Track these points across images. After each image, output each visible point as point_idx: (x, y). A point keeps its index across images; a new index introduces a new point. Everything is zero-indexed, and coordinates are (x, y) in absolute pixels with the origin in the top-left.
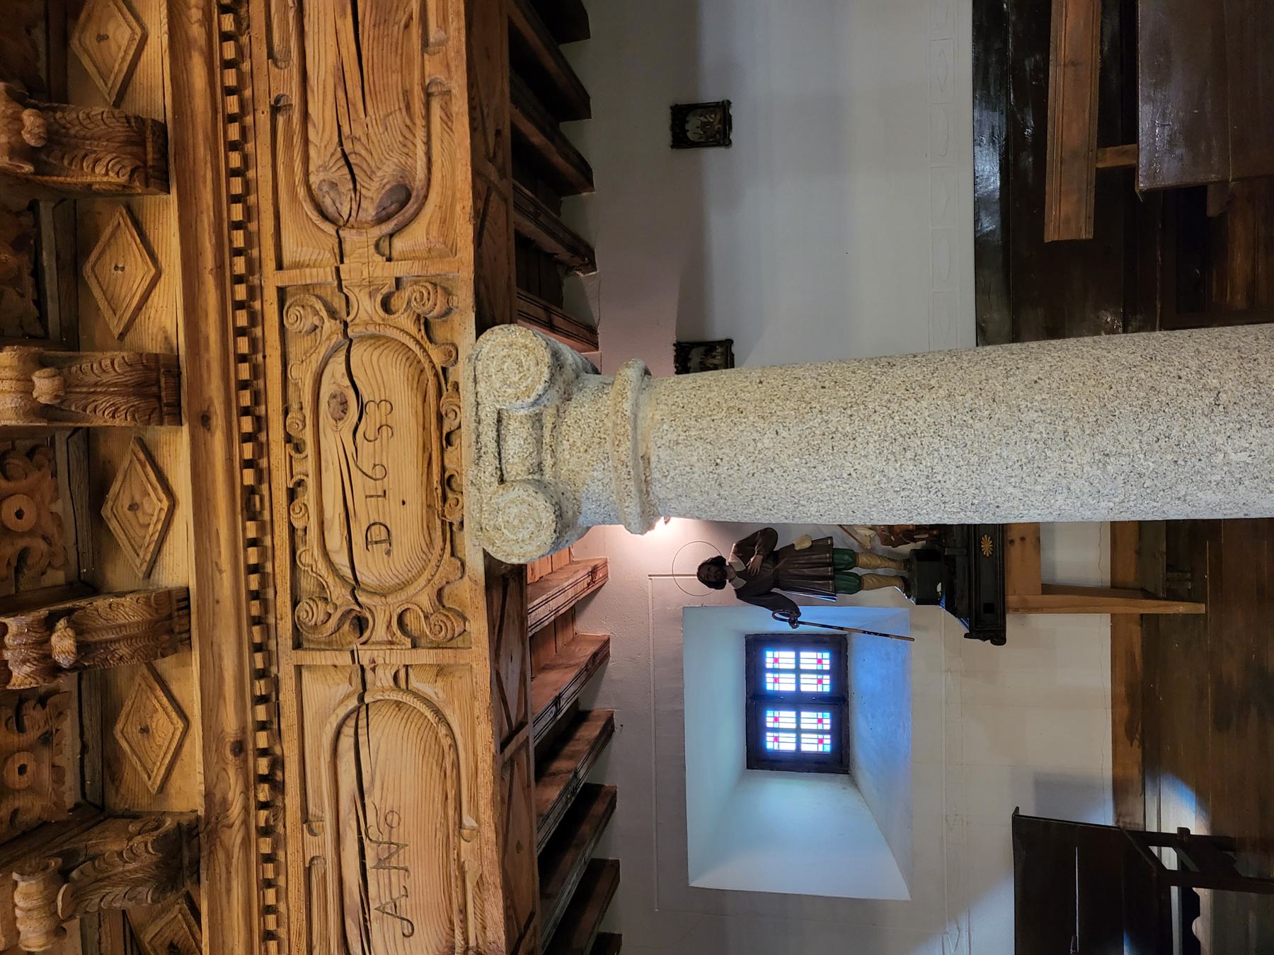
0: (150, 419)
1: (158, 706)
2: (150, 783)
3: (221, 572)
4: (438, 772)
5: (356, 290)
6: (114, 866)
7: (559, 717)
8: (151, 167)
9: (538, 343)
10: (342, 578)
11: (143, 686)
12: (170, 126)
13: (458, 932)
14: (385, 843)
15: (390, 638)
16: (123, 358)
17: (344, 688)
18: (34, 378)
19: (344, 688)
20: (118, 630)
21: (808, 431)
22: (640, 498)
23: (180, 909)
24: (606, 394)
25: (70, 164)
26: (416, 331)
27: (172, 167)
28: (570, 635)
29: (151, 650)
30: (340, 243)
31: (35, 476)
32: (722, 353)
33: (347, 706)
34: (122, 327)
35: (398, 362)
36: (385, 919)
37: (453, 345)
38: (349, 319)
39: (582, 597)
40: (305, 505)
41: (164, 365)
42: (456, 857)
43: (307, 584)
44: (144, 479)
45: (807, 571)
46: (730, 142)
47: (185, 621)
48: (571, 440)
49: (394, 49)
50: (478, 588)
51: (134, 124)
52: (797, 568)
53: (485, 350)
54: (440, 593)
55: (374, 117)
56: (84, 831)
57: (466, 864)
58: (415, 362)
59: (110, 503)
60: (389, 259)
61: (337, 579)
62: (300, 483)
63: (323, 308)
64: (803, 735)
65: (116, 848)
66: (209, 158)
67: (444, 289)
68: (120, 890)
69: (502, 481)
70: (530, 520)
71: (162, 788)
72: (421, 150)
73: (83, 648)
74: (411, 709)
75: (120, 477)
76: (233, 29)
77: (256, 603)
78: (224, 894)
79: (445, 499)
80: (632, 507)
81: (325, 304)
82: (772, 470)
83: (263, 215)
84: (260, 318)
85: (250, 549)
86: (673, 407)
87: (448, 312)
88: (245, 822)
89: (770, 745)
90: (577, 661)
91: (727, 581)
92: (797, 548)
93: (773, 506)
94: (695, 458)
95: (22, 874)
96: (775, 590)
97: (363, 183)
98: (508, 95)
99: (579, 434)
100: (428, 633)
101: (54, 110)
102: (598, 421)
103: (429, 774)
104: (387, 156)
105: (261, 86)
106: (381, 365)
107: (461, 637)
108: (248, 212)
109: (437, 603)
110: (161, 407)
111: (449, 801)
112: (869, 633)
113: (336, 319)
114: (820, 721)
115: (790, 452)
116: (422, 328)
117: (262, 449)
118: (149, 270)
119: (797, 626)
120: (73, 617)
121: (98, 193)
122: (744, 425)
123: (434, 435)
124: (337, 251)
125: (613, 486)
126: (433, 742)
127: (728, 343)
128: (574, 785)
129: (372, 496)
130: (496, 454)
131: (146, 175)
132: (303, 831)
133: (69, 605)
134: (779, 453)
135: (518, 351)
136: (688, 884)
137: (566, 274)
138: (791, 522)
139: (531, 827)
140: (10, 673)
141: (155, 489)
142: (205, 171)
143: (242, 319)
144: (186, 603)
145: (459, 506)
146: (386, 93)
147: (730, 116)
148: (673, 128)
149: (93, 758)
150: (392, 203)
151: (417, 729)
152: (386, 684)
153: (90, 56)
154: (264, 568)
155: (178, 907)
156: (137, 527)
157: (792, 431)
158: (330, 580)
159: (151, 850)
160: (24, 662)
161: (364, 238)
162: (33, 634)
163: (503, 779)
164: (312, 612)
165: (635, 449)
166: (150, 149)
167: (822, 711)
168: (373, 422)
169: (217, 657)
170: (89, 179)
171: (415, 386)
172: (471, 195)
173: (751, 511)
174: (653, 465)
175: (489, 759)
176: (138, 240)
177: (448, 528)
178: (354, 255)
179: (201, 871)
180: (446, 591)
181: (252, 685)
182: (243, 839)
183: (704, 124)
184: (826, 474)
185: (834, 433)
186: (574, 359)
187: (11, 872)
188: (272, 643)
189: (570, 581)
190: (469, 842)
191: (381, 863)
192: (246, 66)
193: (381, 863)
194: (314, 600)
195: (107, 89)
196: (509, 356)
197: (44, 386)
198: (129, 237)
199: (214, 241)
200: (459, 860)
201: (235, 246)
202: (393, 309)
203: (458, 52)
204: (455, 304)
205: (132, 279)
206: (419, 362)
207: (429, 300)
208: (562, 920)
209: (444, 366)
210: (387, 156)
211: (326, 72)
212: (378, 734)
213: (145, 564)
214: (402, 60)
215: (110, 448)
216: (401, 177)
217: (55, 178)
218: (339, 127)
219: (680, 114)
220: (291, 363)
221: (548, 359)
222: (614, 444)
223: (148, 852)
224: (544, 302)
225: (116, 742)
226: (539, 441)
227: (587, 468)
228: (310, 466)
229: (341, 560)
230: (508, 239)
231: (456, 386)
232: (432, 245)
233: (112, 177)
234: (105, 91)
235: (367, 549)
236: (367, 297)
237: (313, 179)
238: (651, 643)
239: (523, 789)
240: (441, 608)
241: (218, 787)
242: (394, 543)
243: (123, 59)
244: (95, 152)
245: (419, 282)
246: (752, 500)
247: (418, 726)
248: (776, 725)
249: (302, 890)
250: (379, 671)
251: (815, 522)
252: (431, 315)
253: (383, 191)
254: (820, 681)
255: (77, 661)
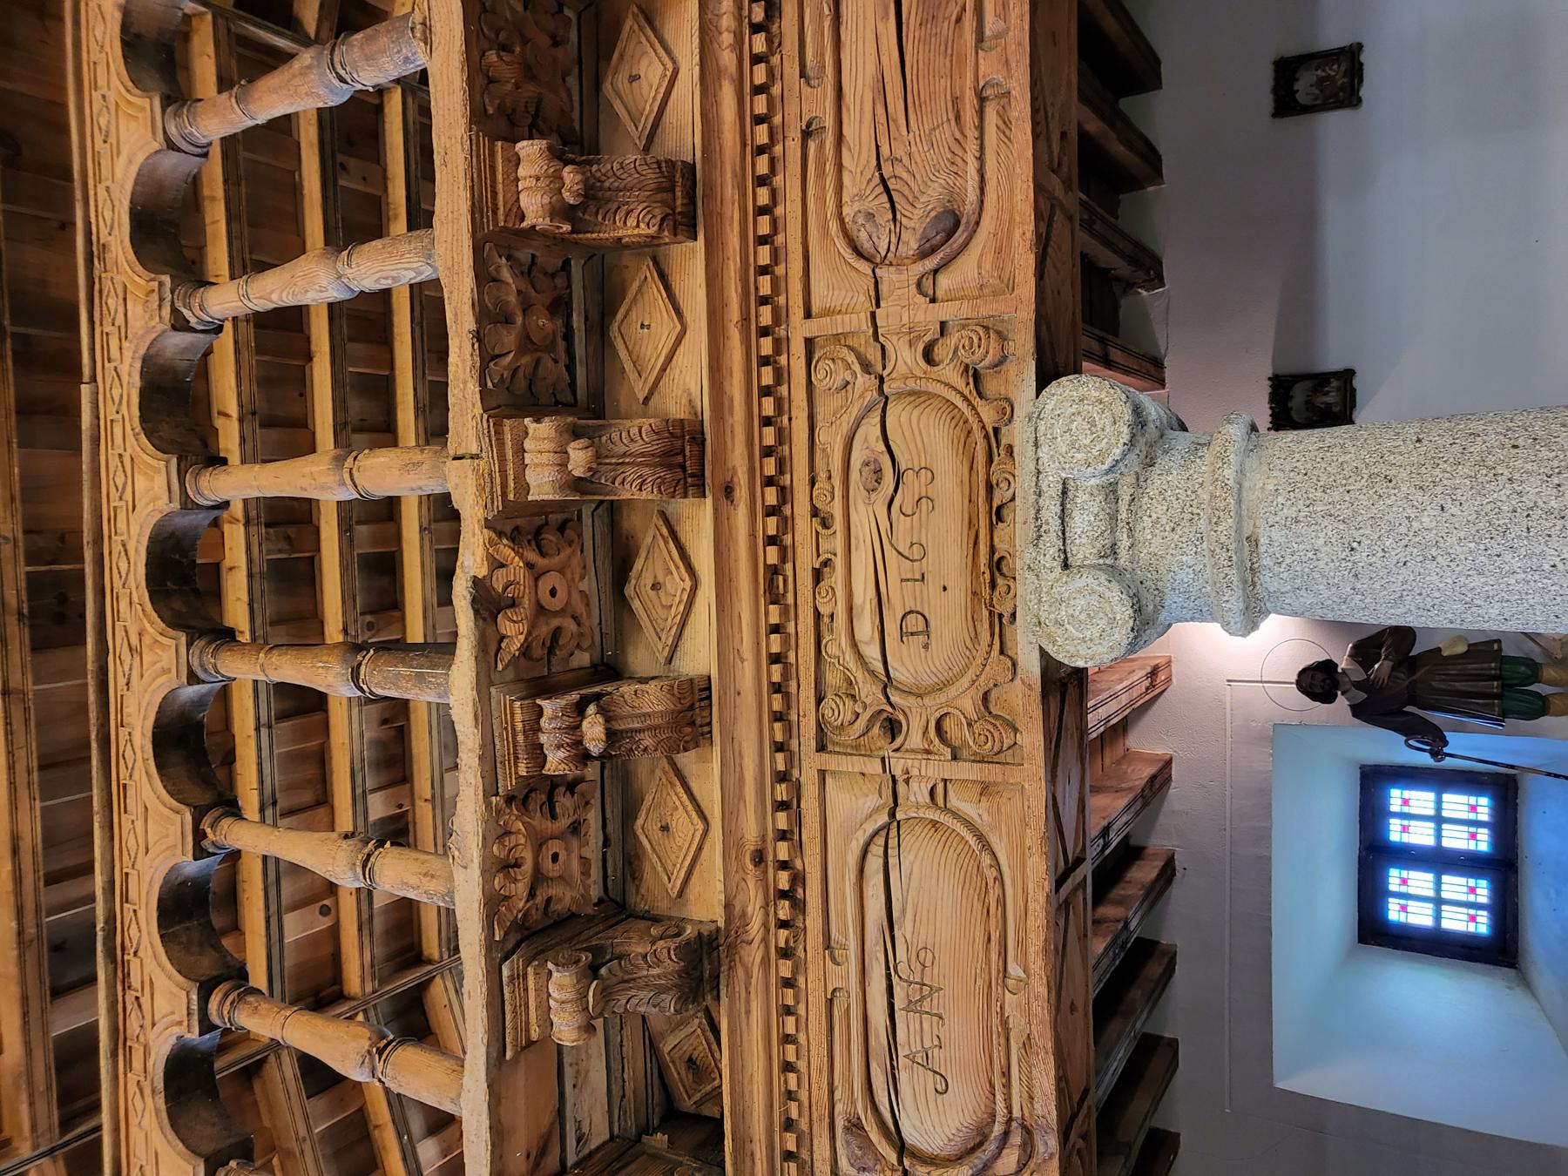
0: (675, 491)
1: (678, 803)
2: (670, 886)
3: (742, 661)
4: (980, 908)
5: (894, 339)
6: (640, 969)
7: (1107, 852)
8: (679, 213)
9: (1115, 396)
10: (873, 673)
11: (664, 780)
12: (698, 167)
13: (999, 1097)
14: (917, 983)
15: (926, 746)
16: (650, 425)
17: (873, 801)
18: (569, 450)
19: (873, 801)
20: (643, 719)
21: (1489, 507)
22: (1244, 590)
23: (700, 1023)
24: (1200, 457)
25: (604, 219)
26: (964, 385)
27: (700, 212)
28: (1120, 751)
29: (675, 742)
30: (876, 283)
31: (567, 552)
32: (1339, 389)
33: (876, 821)
34: (647, 391)
35: (942, 422)
36: (915, 1069)
37: (1007, 400)
38: (885, 373)
39: (1140, 703)
40: (833, 589)
41: (689, 433)
42: (999, 1010)
43: (833, 679)
44: (668, 558)
45: (1459, 686)
46: (1360, 100)
47: (705, 713)
48: (1154, 516)
49: (943, 48)
50: (1033, 693)
51: (664, 169)
52: (1444, 680)
53: (1049, 407)
54: (986, 697)
55: (917, 133)
56: (610, 927)
57: (1011, 1020)
58: (962, 421)
59: (633, 582)
60: (933, 301)
61: (867, 675)
62: (826, 563)
63: (855, 361)
64: (1444, 907)
65: (640, 950)
66: (737, 197)
67: (998, 333)
68: (645, 995)
69: (1066, 566)
70: (1101, 615)
71: (681, 893)
72: (972, 169)
73: (612, 736)
74: (949, 831)
75: (643, 554)
76: (764, 49)
77: (778, 697)
78: (743, 1015)
79: (993, 585)
80: (1234, 601)
81: (859, 356)
82: (1434, 558)
83: (790, 256)
84: (786, 375)
85: (773, 636)
86: (1292, 474)
87: (1002, 360)
88: (765, 940)
89: (1394, 913)
90: (1131, 784)
91: (1339, 693)
92: (1445, 654)
93: (1433, 606)
94: (1321, 541)
95: (557, 965)
96: (1409, 709)
97: (903, 211)
98: (1075, 87)
99: (1165, 508)
100: (971, 743)
101: (590, 163)
102: (1189, 492)
103: (969, 910)
104: (933, 178)
105: (792, 109)
106: (922, 426)
107: (1011, 751)
108: (775, 255)
109: (982, 708)
110: (685, 478)
111: (993, 943)
112: (1557, 776)
113: (870, 374)
114: (1472, 890)
115: (1462, 534)
116: (971, 380)
117: (786, 524)
118: (675, 327)
119: (1442, 759)
120: (602, 702)
121: (627, 246)
122: (1393, 498)
123: (983, 508)
124: (872, 293)
125: (1208, 574)
126: (975, 872)
127: (1348, 374)
128: (1124, 937)
129: (908, 580)
130: (1060, 534)
131: (675, 222)
132: (824, 957)
133: (597, 689)
134: (1444, 535)
135: (1090, 407)
136: (1271, 1085)
137: (1125, 292)
138: (1458, 626)
139: (1087, 986)
140: (545, 757)
141: (677, 568)
142: (733, 211)
143: (767, 376)
144: (707, 693)
145: (1011, 595)
146: (933, 102)
147: (1361, 64)
148: (1276, 90)
149: (615, 853)
150: (937, 234)
151: (956, 856)
152: (920, 800)
153: (621, 99)
154: (786, 657)
155: (696, 1021)
156: (660, 610)
157: (1465, 506)
158: (859, 675)
159: (673, 957)
160: (559, 747)
161: (904, 277)
162: (567, 719)
163: (1058, 925)
164: (837, 711)
165: (1239, 530)
166: (679, 194)
167: (1477, 876)
168: (911, 492)
169: (737, 754)
170: (620, 233)
171: (961, 451)
172: (1033, 217)
173: (1399, 611)
174: (1262, 549)
175: (1042, 900)
176: (665, 295)
177: (997, 620)
178: (894, 297)
179: (721, 987)
180: (994, 695)
181: (773, 788)
182: (763, 958)
183: (1322, 80)
184: (1516, 565)
185: (1531, 509)
186: (1158, 413)
187: (546, 961)
188: (795, 743)
189: (1125, 683)
190: (1015, 994)
191: (911, 1006)
192: (776, 90)
193: (911, 1006)
194: (840, 697)
195: (636, 133)
196: (1079, 413)
197: (579, 458)
198: (655, 291)
199: (739, 290)
200: (1002, 1015)
201: (761, 294)
202: (937, 359)
203: (1020, 44)
204: (1011, 350)
205: (658, 338)
206: (966, 422)
207: (979, 347)
208: (1104, 1105)
209: (996, 425)
210: (933, 178)
211: (864, 85)
212: (911, 857)
213: (667, 649)
214: (951, 61)
215: (633, 522)
216: (949, 201)
217: (589, 235)
218: (877, 147)
219: (1286, 70)
220: (819, 425)
221: (1127, 415)
222: (1210, 522)
223: (670, 958)
224: (1096, 331)
225: (636, 837)
226: (1113, 517)
227: (1174, 552)
228: (838, 544)
229: (872, 652)
230: (1074, 266)
231: (1010, 450)
232: (985, 281)
233: (643, 230)
234: (635, 134)
235: (902, 641)
236: (907, 346)
237: (847, 211)
238: (1228, 768)
239: (1079, 938)
240: (987, 714)
241: (738, 897)
242: (933, 636)
243: (654, 98)
244: (627, 203)
245: (969, 325)
246: (1402, 596)
247: (958, 851)
248: (1403, 889)
249: (824, 1023)
250: (914, 784)
251: (1495, 628)
252: (982, 364)
253: (928, 220)
254: (1473, 836)
255: (605, 750)
